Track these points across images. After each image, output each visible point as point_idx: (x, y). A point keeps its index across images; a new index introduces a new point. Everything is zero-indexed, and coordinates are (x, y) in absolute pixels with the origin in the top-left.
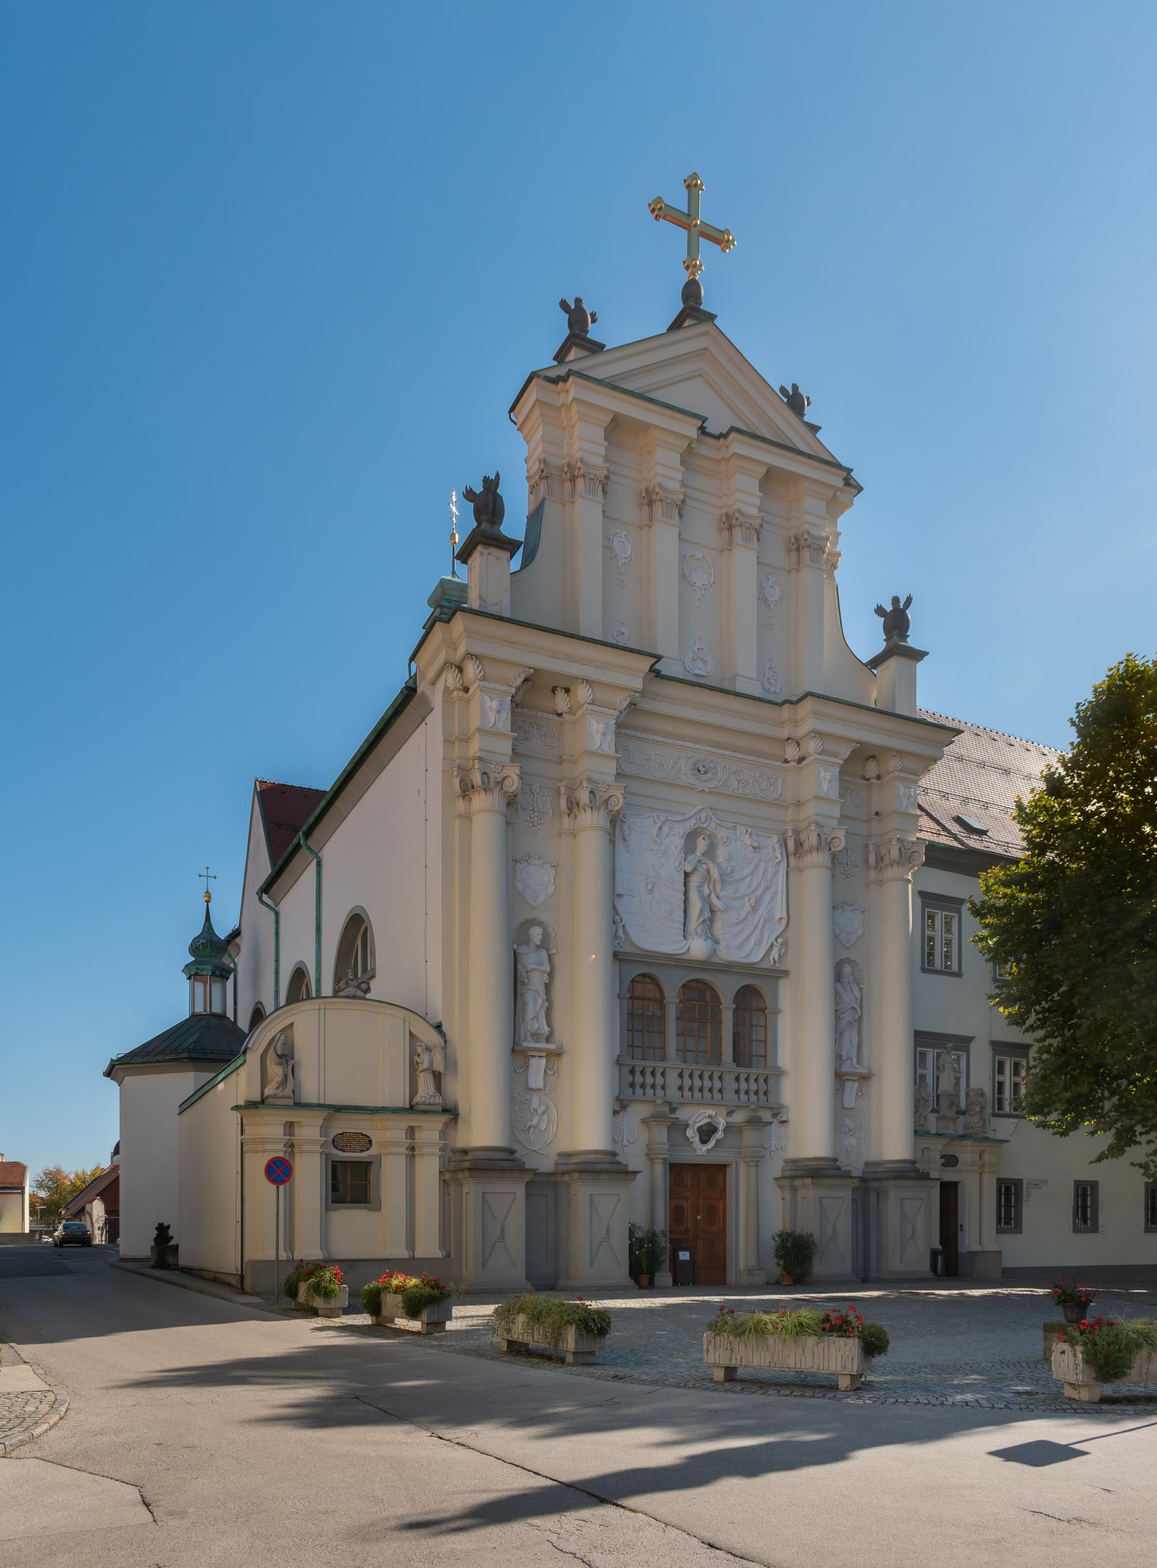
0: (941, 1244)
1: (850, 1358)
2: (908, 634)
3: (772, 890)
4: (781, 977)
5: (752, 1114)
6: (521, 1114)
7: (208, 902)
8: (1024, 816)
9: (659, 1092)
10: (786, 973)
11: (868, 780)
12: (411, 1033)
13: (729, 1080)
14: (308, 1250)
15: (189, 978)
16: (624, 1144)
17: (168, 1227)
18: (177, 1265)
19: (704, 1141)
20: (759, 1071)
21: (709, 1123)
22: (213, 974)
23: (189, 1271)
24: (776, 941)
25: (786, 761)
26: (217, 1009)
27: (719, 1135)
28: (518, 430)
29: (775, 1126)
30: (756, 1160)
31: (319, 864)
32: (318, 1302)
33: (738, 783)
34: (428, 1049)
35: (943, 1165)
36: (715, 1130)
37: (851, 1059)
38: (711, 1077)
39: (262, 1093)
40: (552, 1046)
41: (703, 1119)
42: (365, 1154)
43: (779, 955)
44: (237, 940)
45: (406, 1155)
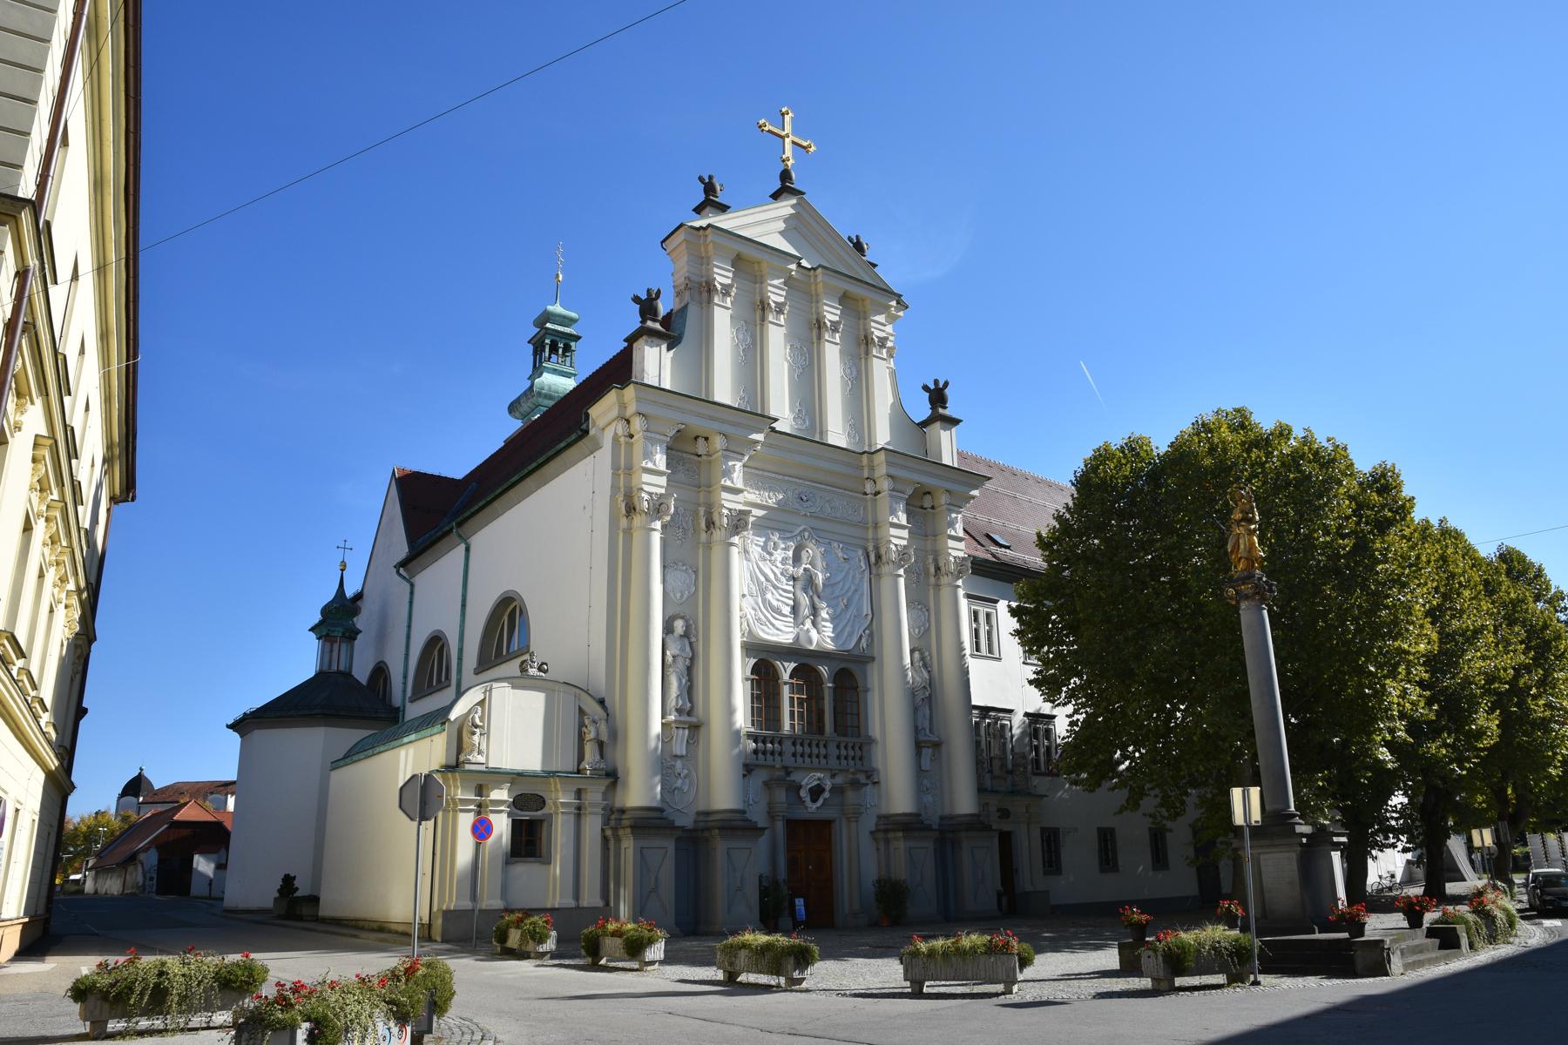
3: (859, 593)
4: (868, 662)
5: (851, 776)
7: (342, 570)
8: (1042, 543)
10: (873, 659)
12: (580, 709)
17: (294, 878)
18: (317, 916)
19: (814, 800)
20: (856, 740)
23: (337, 922)
25: (865, 494)
26: (342, 668)
27: (826, 795)
28: (668, 254)
29: (869, 788)
31: (468, 550)
34: (594, 722)
35: (999, 817)
36: (823, 790)
38: (818, 745)
39: (458, 759)
40: (693, 719)
42: (539, 813)
44: (359, 603)
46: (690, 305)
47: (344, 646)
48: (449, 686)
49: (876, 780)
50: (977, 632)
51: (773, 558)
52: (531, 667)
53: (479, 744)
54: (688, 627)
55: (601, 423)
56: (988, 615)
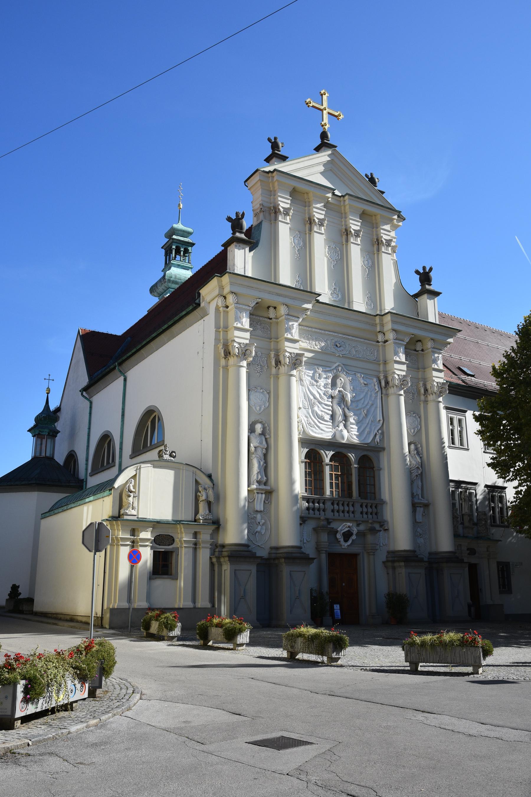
0: (471, 600)
1: (478, 657)
2: (431, 283)
3: (374, 406)
4: (381, 451)
6: (252, 525)
7: (48, 393)
8: (496, 373)
9: (322, 512)
10: (384, 449)
11: (417, 351)
12: (196, 479)
13: (358, 506)
14: (140, 603)
15: (34, 436)
16: (304, 542)
17: (18, 587)
18: (33, 611)
19: (346, 541)
21: (348, 530)
22: (49, 434)
24: (378, 432)
25: (378, 342)
27: (354, 537)
30: (374, 551)
31: (125, 380)
32: (165, 632)
33: (356, 352)
34: (205, 489)
35: (469, 554)
37: (418, 495)
39: (119, 512)
40: (268, 488)
41: (345, 528)
42: (171, 547)
43: (380, 440)
44: (58, 414)
45: (193, 548)
46: (263, 223)
47: (49, 441)
48: (114, 466)
49: (386, 528)
50: (452, 431)
51: (318, 384)
52: (165, 454)
53: (133, 503)
54: (264, 428)
55: (208, 299)
56: (460, 421)
